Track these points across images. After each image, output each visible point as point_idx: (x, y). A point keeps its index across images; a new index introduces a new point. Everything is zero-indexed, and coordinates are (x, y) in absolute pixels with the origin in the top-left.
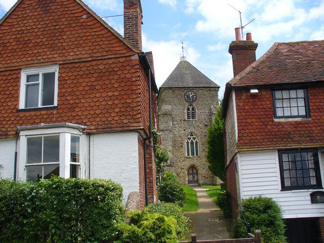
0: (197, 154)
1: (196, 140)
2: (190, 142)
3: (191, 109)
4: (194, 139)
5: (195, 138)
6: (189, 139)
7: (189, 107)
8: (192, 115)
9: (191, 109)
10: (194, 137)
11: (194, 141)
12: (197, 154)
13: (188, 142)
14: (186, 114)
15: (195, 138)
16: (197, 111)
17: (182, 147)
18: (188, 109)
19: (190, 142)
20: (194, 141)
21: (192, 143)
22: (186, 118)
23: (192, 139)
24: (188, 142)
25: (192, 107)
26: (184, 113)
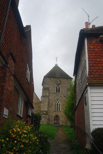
1: (59, 103)
2: (56, 104)
3: (58, 88)
5: (59, 102)
6: (56, 102)
7: (57, 87)
8: (58, 91)
9: (58, 88)
12: (59, 110)
14: (55, 90)
15: (59, 102)
17: (52, 106)
19: (56, 104)
21: (57, 104)
22: (55, 92)
23: (57, 102)
24: (57, 88)
25: (59, 87)
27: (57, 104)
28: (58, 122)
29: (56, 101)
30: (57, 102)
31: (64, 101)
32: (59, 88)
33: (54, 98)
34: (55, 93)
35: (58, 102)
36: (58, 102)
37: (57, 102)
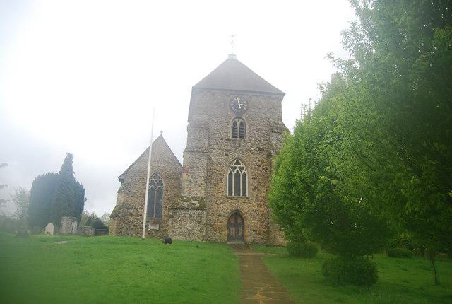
0: (244, 194)
2: (234, 173)
3: (238, 124)
4: (241, 169)
5: (243, 168)
7: (237, 120)
9: (238, 124)
10: (241, 166)
11: (242, 173)
12: (244, 194)
13: (231, 174)
14: (230, 131)
15: (243, 168)
16: (248, 127)
18: (235, 124)
19: (234, 173)
20: (242, 173)
21: (238, 175)
23: (237, 169)
24: (235, 124)
26: (228, 129)
27: (238, 175)
28: (240, 233)
29: (234, 165)
30: (235, 168)
31: (260, 166)
32: (241, 124)
33: (226, 155)
34: (228, 140)
35: (240, 168)
36: (240, 168)
37: (237, 169)
